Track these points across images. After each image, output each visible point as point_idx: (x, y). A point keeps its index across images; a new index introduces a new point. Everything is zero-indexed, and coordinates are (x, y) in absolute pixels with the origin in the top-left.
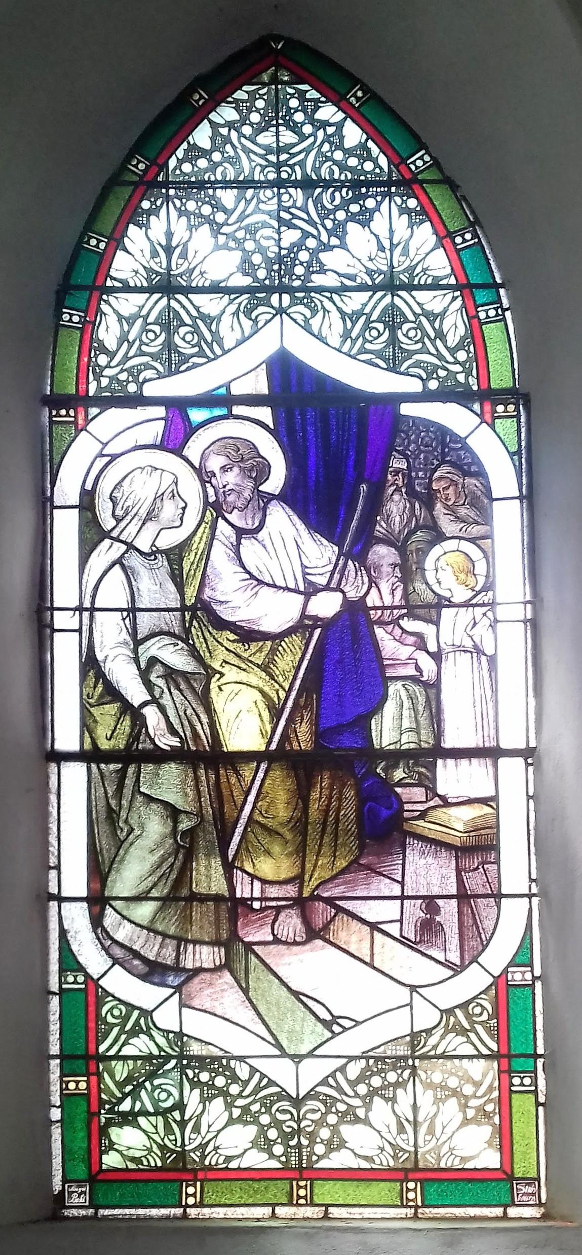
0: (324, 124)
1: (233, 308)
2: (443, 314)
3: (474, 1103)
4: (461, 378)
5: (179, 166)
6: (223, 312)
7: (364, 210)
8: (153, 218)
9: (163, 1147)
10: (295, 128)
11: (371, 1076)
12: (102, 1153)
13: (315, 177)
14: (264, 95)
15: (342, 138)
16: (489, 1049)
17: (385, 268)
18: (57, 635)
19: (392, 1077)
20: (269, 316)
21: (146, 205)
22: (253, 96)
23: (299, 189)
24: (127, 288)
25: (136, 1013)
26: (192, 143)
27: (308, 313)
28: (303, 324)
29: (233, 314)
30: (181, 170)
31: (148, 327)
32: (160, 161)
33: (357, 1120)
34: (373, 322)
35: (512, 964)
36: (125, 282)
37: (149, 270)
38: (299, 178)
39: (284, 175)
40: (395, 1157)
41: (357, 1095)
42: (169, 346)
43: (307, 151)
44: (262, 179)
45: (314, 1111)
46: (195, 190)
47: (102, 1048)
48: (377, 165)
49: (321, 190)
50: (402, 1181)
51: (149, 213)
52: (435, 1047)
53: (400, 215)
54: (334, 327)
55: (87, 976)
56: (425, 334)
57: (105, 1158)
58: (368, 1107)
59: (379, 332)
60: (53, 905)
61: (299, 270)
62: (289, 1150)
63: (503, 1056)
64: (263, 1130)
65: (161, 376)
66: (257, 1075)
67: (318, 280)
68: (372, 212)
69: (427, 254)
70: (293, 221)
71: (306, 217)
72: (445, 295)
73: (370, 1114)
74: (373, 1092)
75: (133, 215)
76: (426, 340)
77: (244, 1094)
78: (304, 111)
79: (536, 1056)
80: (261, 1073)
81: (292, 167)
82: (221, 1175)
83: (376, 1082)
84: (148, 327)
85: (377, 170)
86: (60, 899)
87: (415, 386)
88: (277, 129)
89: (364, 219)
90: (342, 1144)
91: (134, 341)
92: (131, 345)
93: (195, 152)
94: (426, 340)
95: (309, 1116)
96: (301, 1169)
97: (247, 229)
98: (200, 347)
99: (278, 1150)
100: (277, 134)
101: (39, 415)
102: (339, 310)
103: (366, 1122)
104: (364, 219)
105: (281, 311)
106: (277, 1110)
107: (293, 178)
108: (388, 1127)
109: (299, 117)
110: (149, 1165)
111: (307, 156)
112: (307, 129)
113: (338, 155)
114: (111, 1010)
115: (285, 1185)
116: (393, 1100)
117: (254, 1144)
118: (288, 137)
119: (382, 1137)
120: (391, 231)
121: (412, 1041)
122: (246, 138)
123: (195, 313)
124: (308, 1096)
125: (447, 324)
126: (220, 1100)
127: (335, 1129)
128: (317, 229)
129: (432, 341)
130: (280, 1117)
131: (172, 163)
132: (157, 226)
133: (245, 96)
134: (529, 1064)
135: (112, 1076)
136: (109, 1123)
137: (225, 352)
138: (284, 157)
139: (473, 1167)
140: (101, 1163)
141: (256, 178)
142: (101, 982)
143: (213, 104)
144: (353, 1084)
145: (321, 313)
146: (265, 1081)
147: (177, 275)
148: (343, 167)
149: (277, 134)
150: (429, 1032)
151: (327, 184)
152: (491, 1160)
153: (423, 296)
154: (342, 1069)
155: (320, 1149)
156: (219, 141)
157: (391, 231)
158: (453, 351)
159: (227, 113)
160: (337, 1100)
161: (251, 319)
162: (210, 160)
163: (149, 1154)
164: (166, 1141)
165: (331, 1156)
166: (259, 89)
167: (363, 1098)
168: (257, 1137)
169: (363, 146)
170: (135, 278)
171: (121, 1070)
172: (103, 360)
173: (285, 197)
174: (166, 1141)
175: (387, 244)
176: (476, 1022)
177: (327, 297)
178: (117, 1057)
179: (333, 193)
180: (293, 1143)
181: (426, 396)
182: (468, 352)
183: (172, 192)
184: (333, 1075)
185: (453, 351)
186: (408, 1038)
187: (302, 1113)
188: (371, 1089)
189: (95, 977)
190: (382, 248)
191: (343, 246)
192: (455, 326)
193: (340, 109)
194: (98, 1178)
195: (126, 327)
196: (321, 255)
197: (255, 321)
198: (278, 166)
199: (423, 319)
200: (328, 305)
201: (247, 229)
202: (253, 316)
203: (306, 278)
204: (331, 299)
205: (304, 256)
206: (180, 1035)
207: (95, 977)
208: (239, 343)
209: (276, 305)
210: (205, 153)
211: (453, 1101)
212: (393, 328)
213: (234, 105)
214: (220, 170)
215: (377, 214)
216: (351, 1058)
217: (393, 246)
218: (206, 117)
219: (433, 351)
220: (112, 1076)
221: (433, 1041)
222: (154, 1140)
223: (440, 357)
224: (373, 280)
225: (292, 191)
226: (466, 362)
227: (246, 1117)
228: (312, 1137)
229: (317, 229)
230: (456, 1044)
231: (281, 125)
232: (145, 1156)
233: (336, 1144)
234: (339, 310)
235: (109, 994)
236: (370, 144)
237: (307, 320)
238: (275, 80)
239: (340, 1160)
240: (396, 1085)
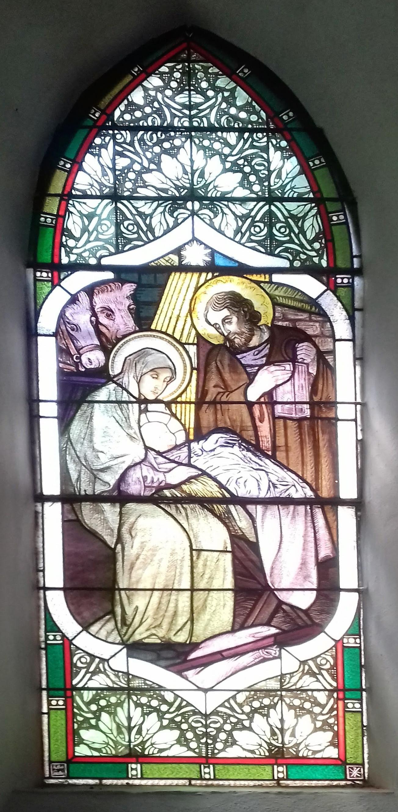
0: (222, 90)
1: (161, 209)
2: (151, 216)
3: (321, 718)
4: (316, 260)
5: (121, 116)
6: (306, 214)
7: (173, 147)
8: (103, 150)
9: (269, 744)
10: (203, 93)
11: (100, 699)
12: (75, 745)
13: (217, 125)
14: (180, 69)
15: (235, 98)
16: (331, 685)
17: (188, 185)
18: (339, 423)
19: (266, 701)
20: (186, 216)
21: (98, 141)
22: (172, 70)
23: (128, 132)
24: (85, 196)
25: (97, 660)
26: (130, 100)
27: (212, 215)
28: (208, 222)
29: (161, 213)
30: (123, 118)
31: (102, 222)
32: (108, 112)
33: (244, 728)
34: (104, 219)
35: (347, 634)
36: (84, 191)
37: (101, 184)
38: (206, 125)
39: (195, 124)
40: (115, 748)
41: (243, 713)
42: (270, 235)
43: (212, 107)
44: (180, 125)
45: (216, 722)
46: (208, 133)
47: (74, 682)
48: (259, 117)
49: (143, 132)
50: (273, 765)
51: (101, 146)
52: (295, 684)
53: (275, 152)
54: (230, 224)
55: (64, 636)
56: (292, 230)
57: (77, 749)
58: (251, 719)
59: (108, 227)
60: (117, 592)
61: (129, 185)
62: (201, 745)
63: (340, 690)
64: (183, 733)
65: (111, 254)
66: (179, 699)
67: (143, 192)
68: (179, 148)
69: (166, 177)
70: (124, 152)
71: (133, 150)
72: (305, 205)
73: (252, 724)
74: (255, 711)
75: (87, 147)
76: (292, 235)
77: (171, 711)
78: (208, 81)
79: (361, 690)
80: (182, 698)
81: (201, 118)
82: (312, 762)
83: (256, 704)
84: (102, 222)
85: (260, 121)
86: (46, 589)
87: (284, 264)
88: (190, 93)
89: (173, 152)
90: (234, 743)
91: (93, 232)
92: (90, 234)
93: (132, 107)
94: (292, 235)
95: (212, 725)
96: (207, 757)
97: (245, 158)
98: (139, 234)
99: (193, 745)
100: (190, 96)
101: (25, 277)
102: (233, 213)
103: (250, 729)
104: (173, 152)
105: (193, 213)
106: (193, 721)
107: (202, 125)
108: (264, 732)
109: (204, 85)
110: (107, 753)
111: (211, 111)
112: (210, 93)
113: (233, 111)
114: (79, 659)
115: (197, 767)
116: (267, 716)
117: (178, 741)
118: (197, 99)
119: (261, 738)
120: (192, 161)
121: (281, 679)
122: (168, 98)
123: (134, 212)
124: (212, 713)
125: (307, 224)
126: (154, 715)
127: (230, 734)
128: (141, 158)
129: (297, 236)
130: (194, 724)
131: (117, 113)
132: (107, 155)
133: (167, 70)
134: (357, 694)
135: (82, 698)
136: (80, 728)
137: (156, 238)
138: (194, 112)
139: (320, 757)
140: (74, 752)
141: (176, 125)
142: (74, 642)
143: (147, 74)
144: (241, 706)
145: (221, 215)
146: (184, 703)
147: (198, 188)
148: (236, 118)
149: (190, 96)
150: (292, 674)
151: (154, 129)
152: (333, 752)
153: (291, 206)
154: (234, 697)
155: (219, 746)
156: (150, 101)
157: (192, 161)
158: (311, 243)
159: (155, 81)
160: (230, 716)
161: (173, 217)
162: (143, 112)
163: (107, 746)
164: (118, 738)
165: (227, 750)
166: (176, 65)
167: (247, 714)
168: (180, 737)
169: (248, 104)
170: (91, 189)
171: (88, 696)
172: (71, 243)
173: (118, 136)
174: (118, 738)
175: (189, 170)
176: (323, 669)
177: (225, 205)
178: (84, 688)
179: (152, 134)
180: (204, 740)
181: (291, 270)
182: (321, 243)
183: (193, 134)
184: (228, 701)
185: (311, 243)
186: (279, 677)
187: (208, 722)
188: (253, 709)
189: (70, 638)
190: (185, 172)
191: (159, 170)
192: (312, 226)
193: (232, 80)
194: (72, 760)
195: (240, 223)
196: (144, 176)
197: (176, 219)
198: (191, 117)
199: (138, 218)
200: (226, 210)
201: (245, 158)
202: (175, 214)
203: (135, 191)
204: (227, 206)
205: (132, 176)
206: (127, 674)
207: (70, 638)
208: (165, 233)
209: (190, 208)
210: (140, 108)
211: (308, 717)
212: (271, 226)
213: (159, 76)
214: (150, 119)
215: (182, 149)
216: (239, 691)
217: (193, 173)
218: (140, 84)
219: (297, 241)
220: (82, 698)
221: (294, 680)
222: (110, 738)
223: (301, 245)
224: (180, 193)
225: (123, 132)
226: (319, 250)
227: (174, 725)
228: (215, 739)
229: (141, 158)
230: (308, 682)
231: (193, 90)
232: (104, 748)
233: (231, 742)
234: (233, 213)
235: (78, 648)
236: (254, 104)
237: (211, 220)
238: (189, 60)
239: (233, 752)
240: (269, 707)
